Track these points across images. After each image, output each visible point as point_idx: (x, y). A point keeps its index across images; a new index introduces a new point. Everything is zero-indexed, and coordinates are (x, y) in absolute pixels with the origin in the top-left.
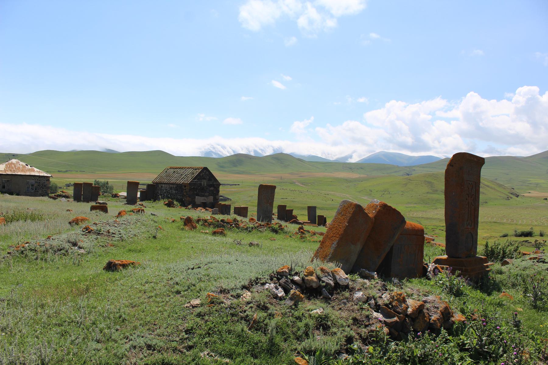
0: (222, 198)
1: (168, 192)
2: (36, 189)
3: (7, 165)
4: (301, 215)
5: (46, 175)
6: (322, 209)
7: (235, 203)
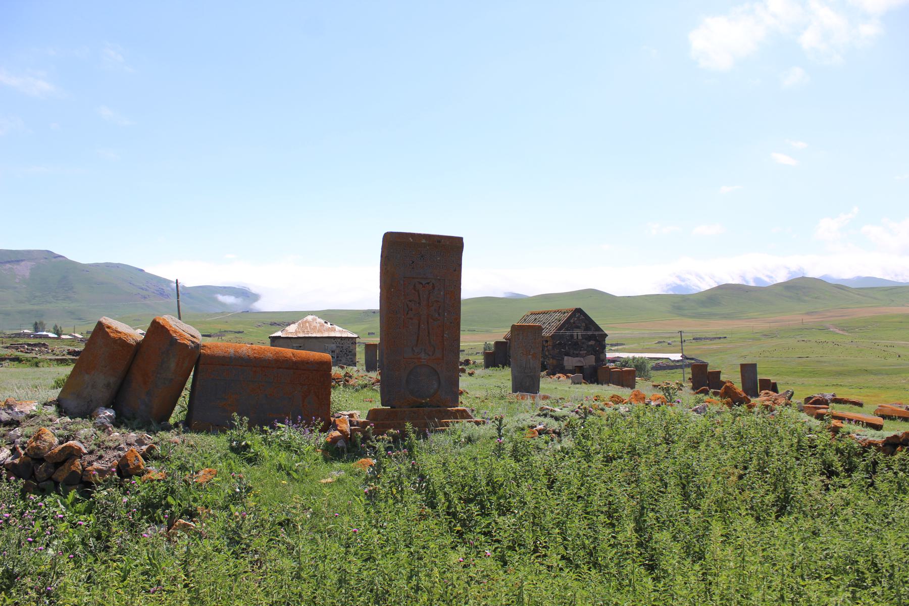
0: (693, 361)
2: (337, 357)
3: (299, 325)
4: (833, 385)
5: (350, 335)
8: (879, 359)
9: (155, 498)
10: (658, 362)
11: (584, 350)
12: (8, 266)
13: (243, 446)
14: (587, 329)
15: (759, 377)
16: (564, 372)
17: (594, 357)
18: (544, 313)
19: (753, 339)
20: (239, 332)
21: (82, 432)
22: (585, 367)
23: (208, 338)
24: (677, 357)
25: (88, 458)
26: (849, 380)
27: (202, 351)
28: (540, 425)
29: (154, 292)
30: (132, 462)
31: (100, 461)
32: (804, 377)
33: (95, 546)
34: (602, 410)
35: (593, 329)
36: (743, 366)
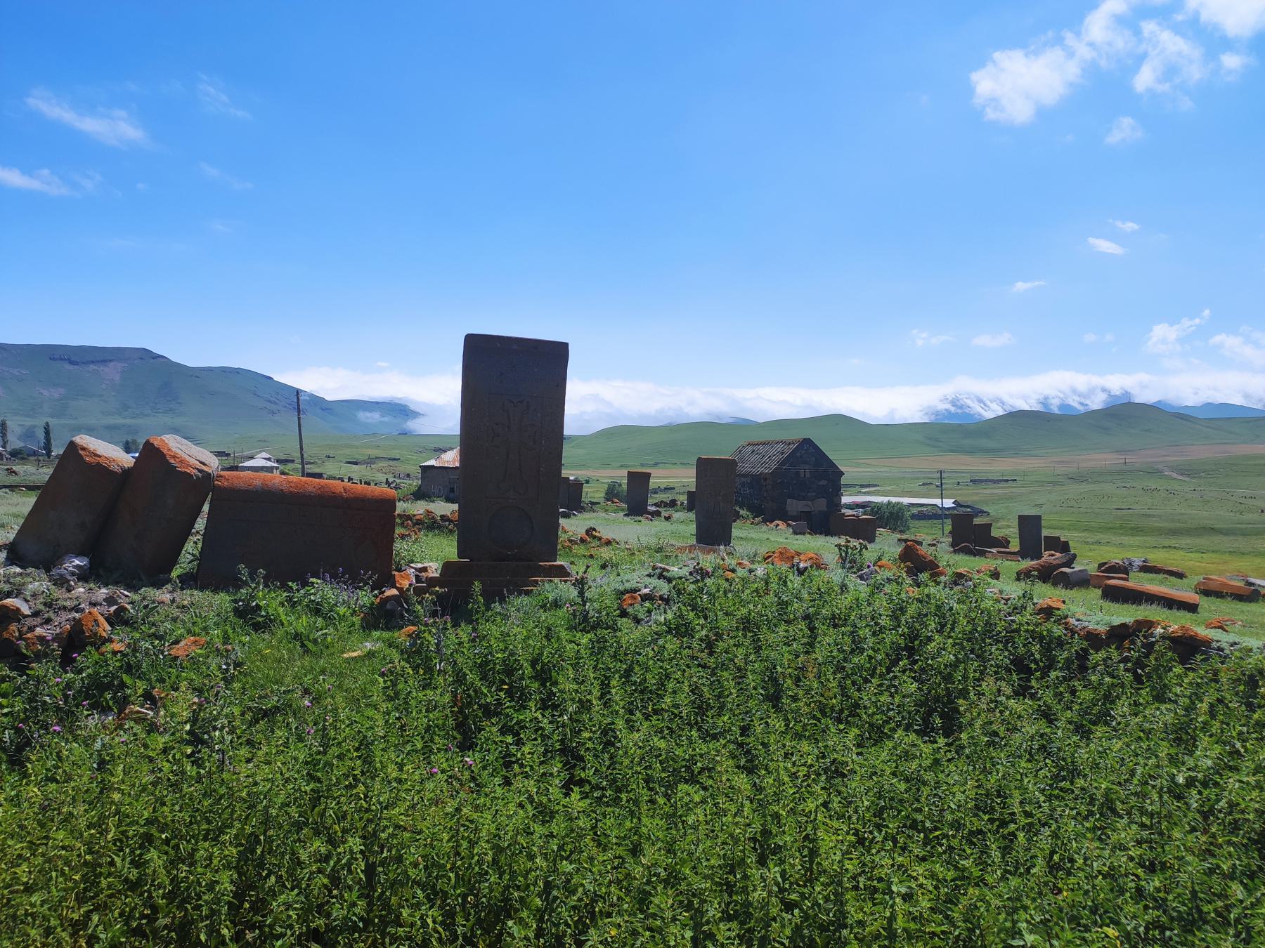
0: (969, 510)
4: (1164, 547)
9: (105, 676)
10: (920, 509)
12: (92, 367)
13: (253, 607)
15: (1045, 533)
16: (785, 518)
18: (764, 444)
19: (1055, 483)
20: (394, 459)
21: (30, 586)
23: (355, 466)
24: (948, 503)
25: (30, 622)
26: (1186, 541)
27: (216, 482)
28: (645, 588)
29: (285, 407)
30: (88, 626)
31: (45, 626)
32: (1122, 534)
33: (11, 741)
34: (733, 571)
36: (1022, 519)
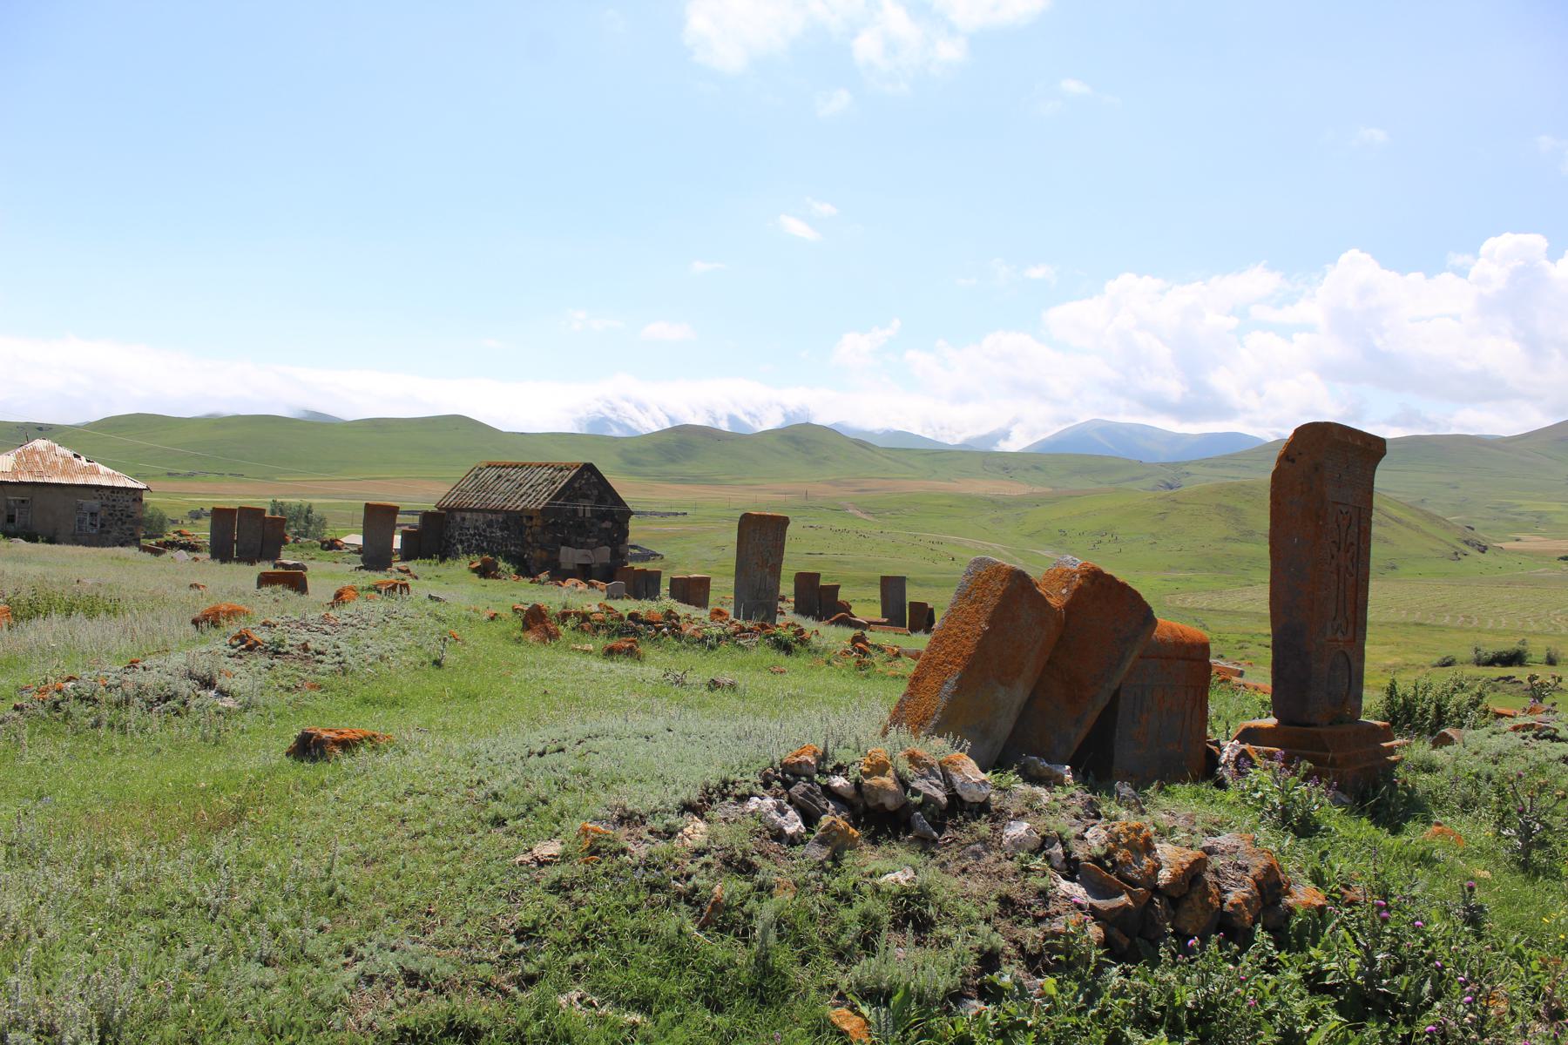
0: (636, 551)
1: (480, 535)
2: (102, 526)
3: (19, 456)
4: (863, 601)
6: (921, 584)
7: (674, 567)
8: (926, 562)
11: (594, 537)
14: (600, 500)
17: (609, 549)
22: (593, 566)
35: (610, 500)
